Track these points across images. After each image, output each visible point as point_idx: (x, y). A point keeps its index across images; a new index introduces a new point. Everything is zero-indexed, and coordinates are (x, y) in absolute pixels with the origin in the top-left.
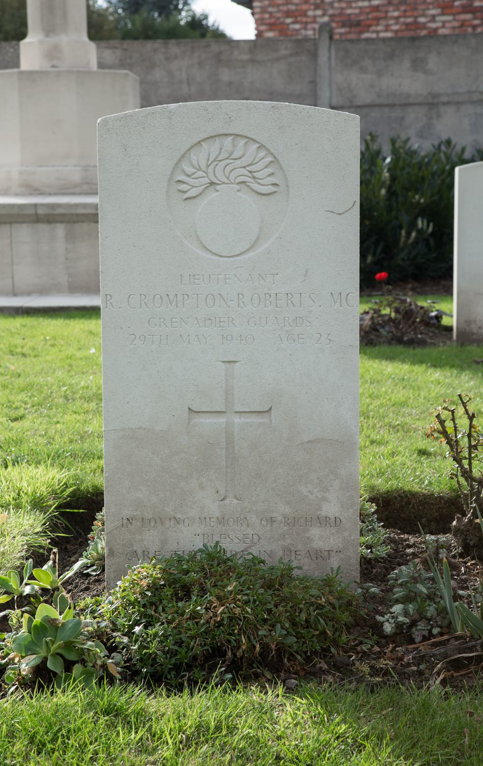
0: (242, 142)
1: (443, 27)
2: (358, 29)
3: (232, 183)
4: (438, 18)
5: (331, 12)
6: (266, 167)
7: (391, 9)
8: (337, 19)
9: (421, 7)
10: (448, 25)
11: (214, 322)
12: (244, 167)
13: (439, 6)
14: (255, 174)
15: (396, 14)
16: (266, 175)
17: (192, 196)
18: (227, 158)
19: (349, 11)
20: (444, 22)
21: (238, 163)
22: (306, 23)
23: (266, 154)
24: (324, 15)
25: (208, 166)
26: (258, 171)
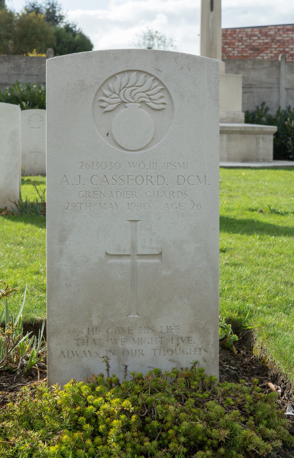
0: (142, 76)
1: (254, 42)
2: (258, 52)
3: (136, 102)
5: (245, 44)
6: (159, 92)
7: (273, 44)
8: (248, 47)
9: (287, 44)
11: (123, 194)
14: (151, 97)
15: (275, 46)
16: (159, 97)
17: (108, 110)
19: (254, 44)
21: (141, 89)
22: (234, 48)
23: (158, 84)
24: (243, 45)
26: (154, 95)
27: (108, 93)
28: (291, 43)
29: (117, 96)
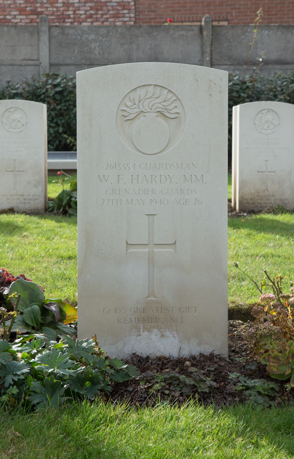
1: (21, 22)
4: (17, 17)
9: (8, 10)
10: (23, 21)
12: (160, 103)
13: (18, 10)
18: (151, 98)
20: (21, 19)
23: (172, 96)
25: (140, 102)
27: (129, 104)
28: (13, 8)
29: (137, 107)
